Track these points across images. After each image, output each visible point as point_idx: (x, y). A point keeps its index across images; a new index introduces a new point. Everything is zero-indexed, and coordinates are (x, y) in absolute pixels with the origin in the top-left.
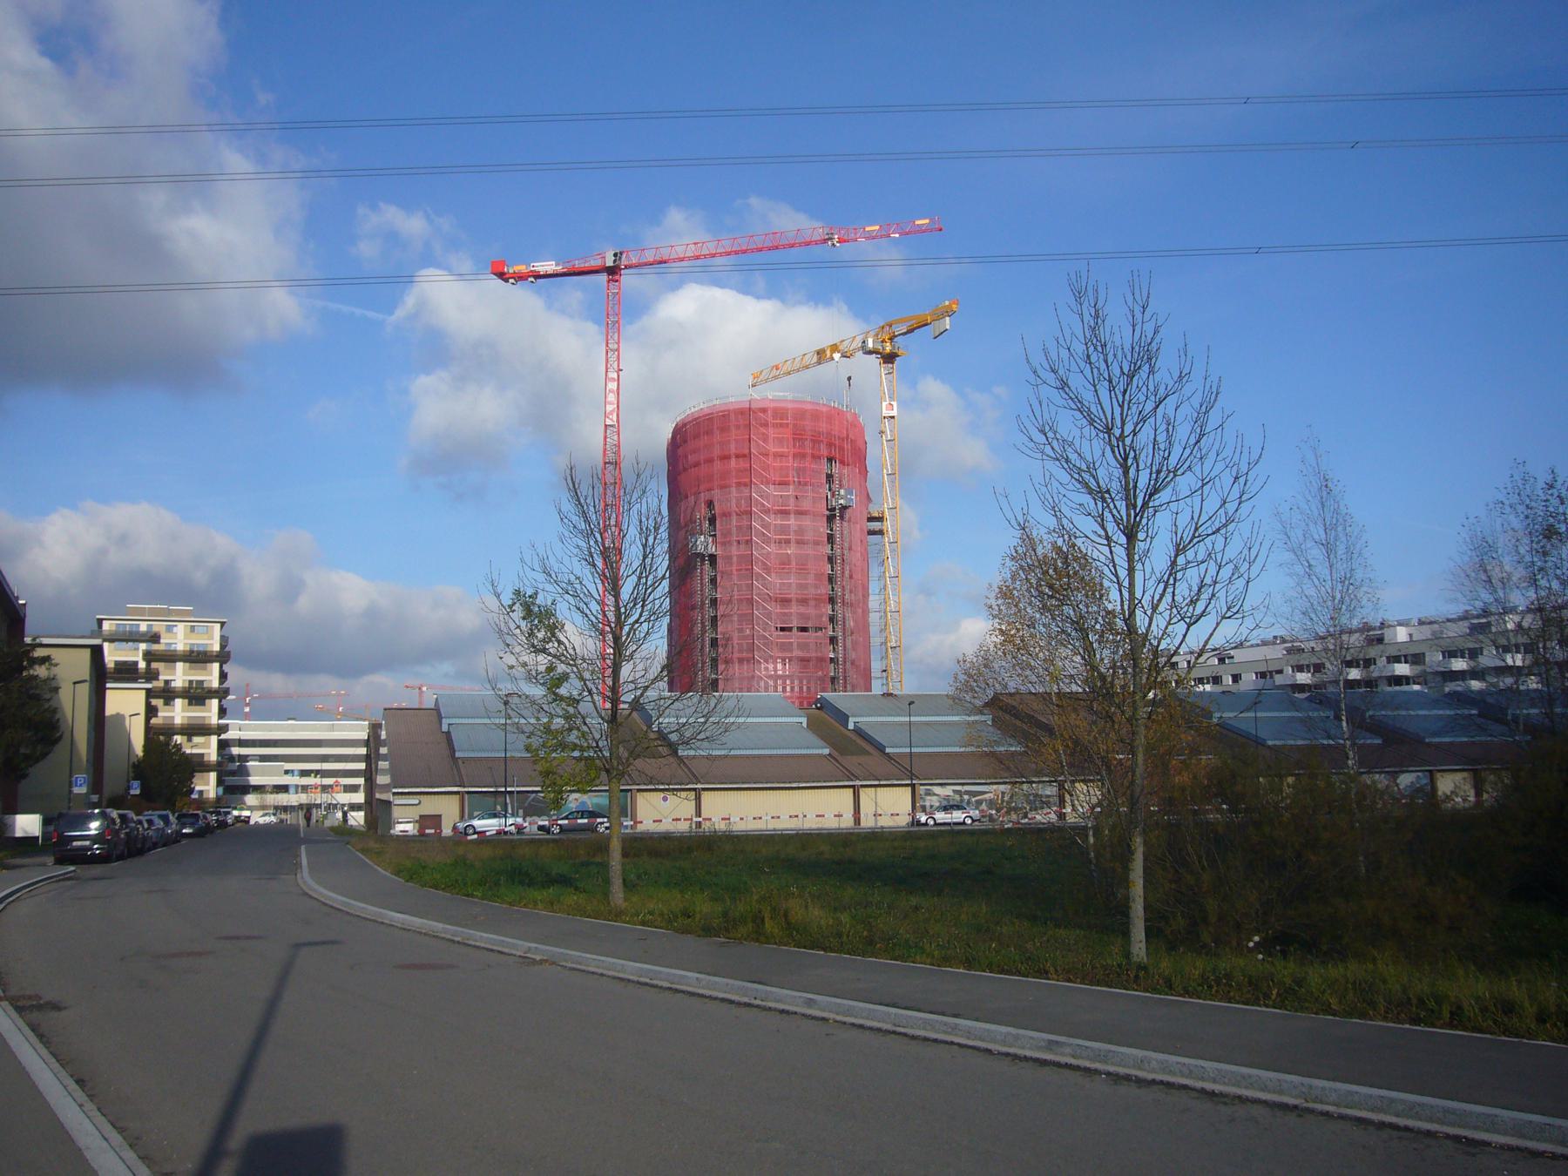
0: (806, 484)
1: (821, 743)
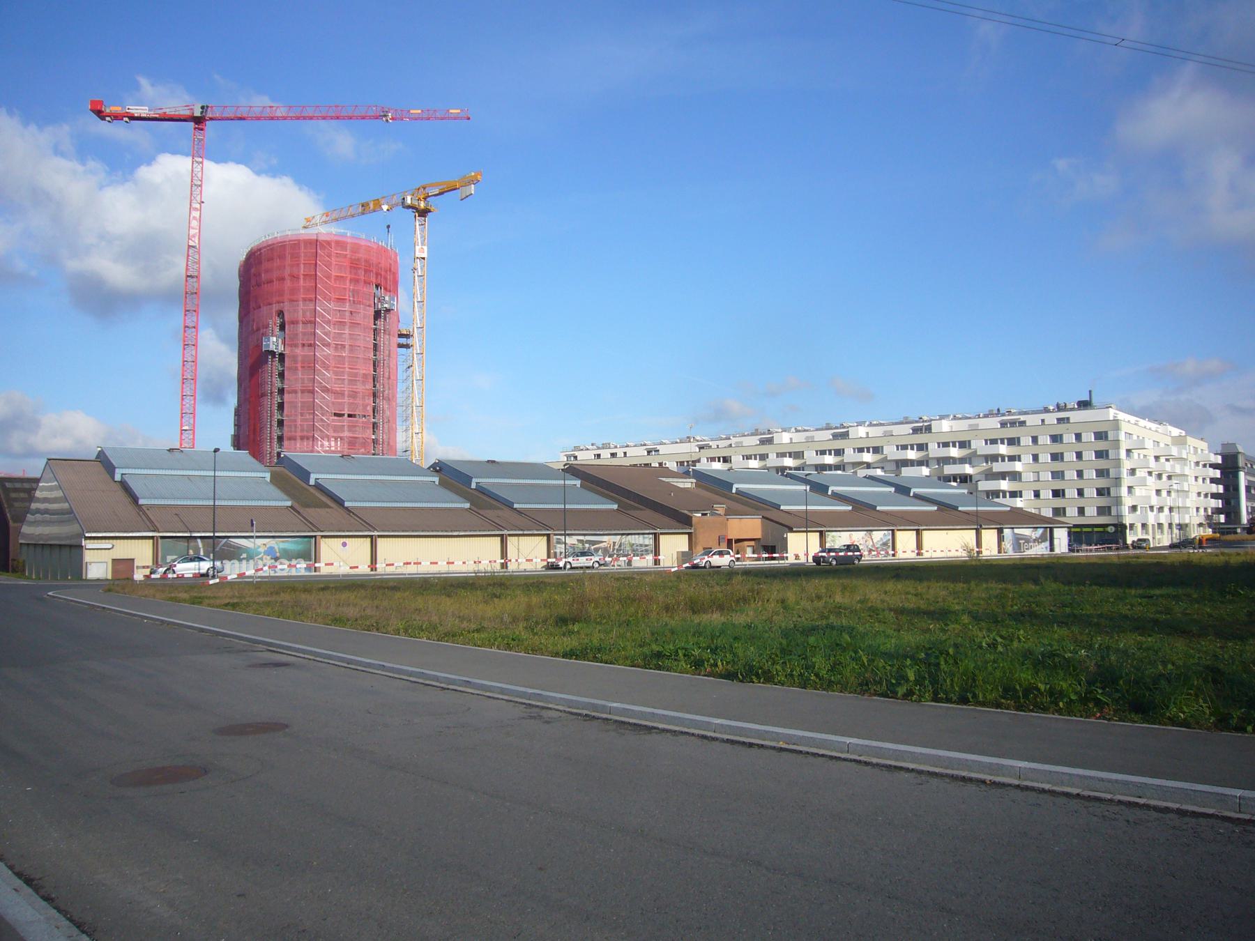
0: (359, 303)
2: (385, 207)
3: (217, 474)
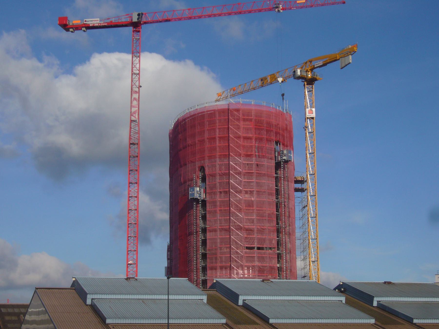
0: (263, 157)
1: (221, 316)
2: (280, 80)
3: (171, 297)
